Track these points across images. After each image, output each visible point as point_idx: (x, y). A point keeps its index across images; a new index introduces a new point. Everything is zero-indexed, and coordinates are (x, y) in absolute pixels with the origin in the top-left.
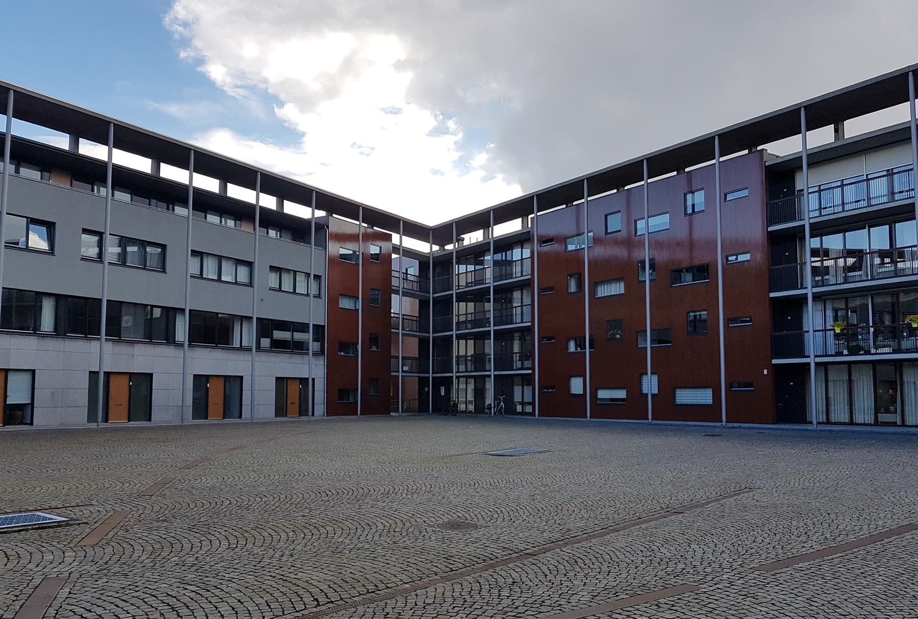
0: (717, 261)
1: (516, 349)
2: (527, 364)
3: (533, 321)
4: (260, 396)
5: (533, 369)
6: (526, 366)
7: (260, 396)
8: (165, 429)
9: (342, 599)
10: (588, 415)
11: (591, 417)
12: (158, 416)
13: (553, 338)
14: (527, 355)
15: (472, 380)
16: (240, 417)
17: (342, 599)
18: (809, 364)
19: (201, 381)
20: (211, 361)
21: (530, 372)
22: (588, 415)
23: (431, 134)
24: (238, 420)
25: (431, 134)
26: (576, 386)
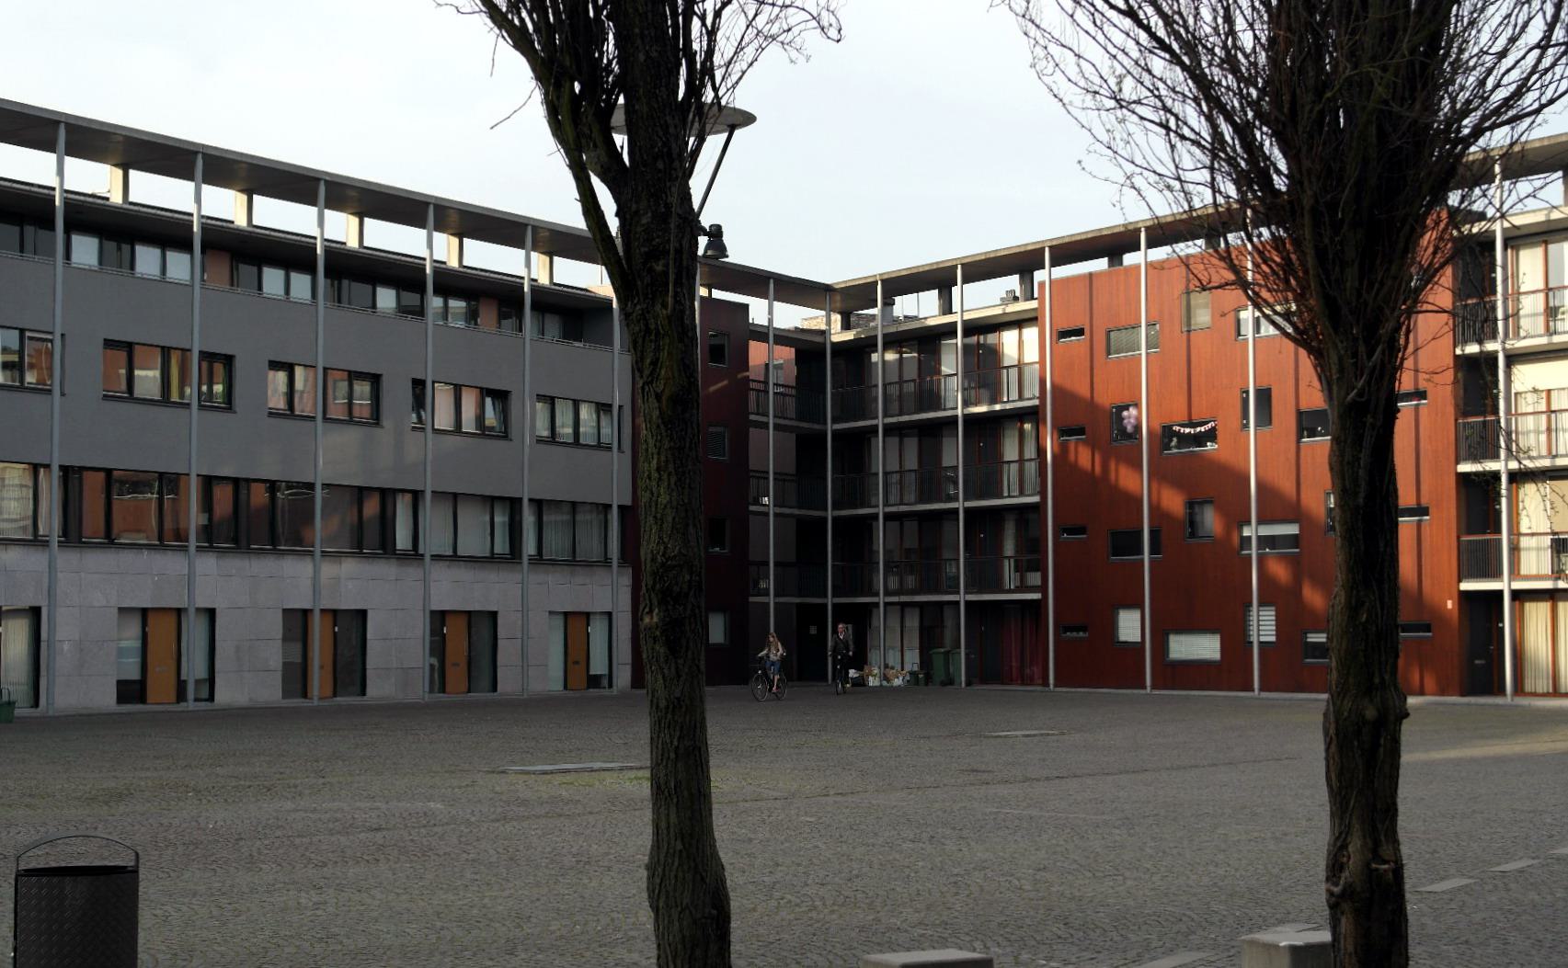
0: (1142, 530)
1: (1009, 548)
2: (1034, 578)
3: (1043, 493)
4: (397, 652)
5: (1043, 588)
6: (1039, 582)
7: (397, 652)
8: (395, 711)
9: (1179, 179)
10: (1256, 685)
11: (1261, 689)
12: (379, 687)
13: (1082, 530)
14: (1031, 558)
15: (917, 612)
16: (494, 689)
17: (1179, 179)
18: (1500, 593)
19: (297, 621)
20: (296, 580)
21: (1036, 596)
22: (1256, 685)
23: (748, 119)
24: (490, 695)
25: (748, 119)
26: (1130, 626)
